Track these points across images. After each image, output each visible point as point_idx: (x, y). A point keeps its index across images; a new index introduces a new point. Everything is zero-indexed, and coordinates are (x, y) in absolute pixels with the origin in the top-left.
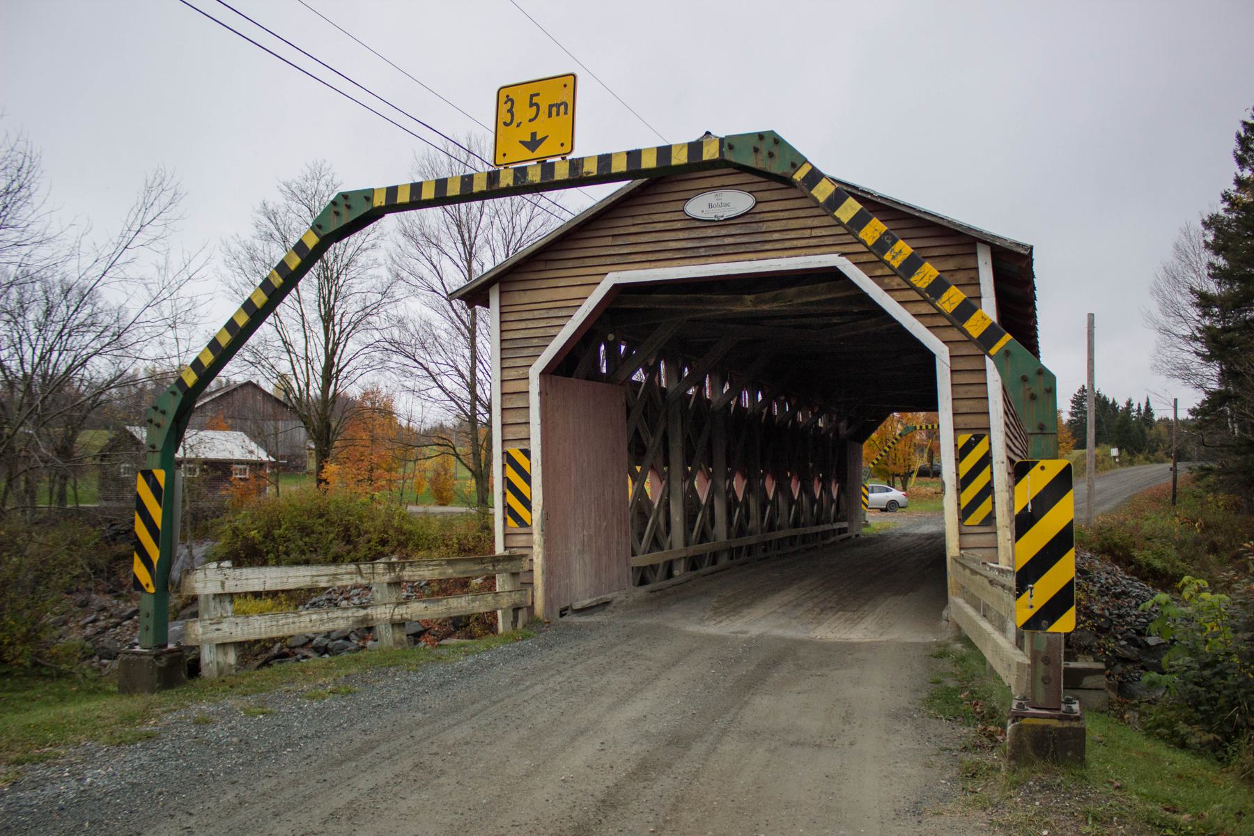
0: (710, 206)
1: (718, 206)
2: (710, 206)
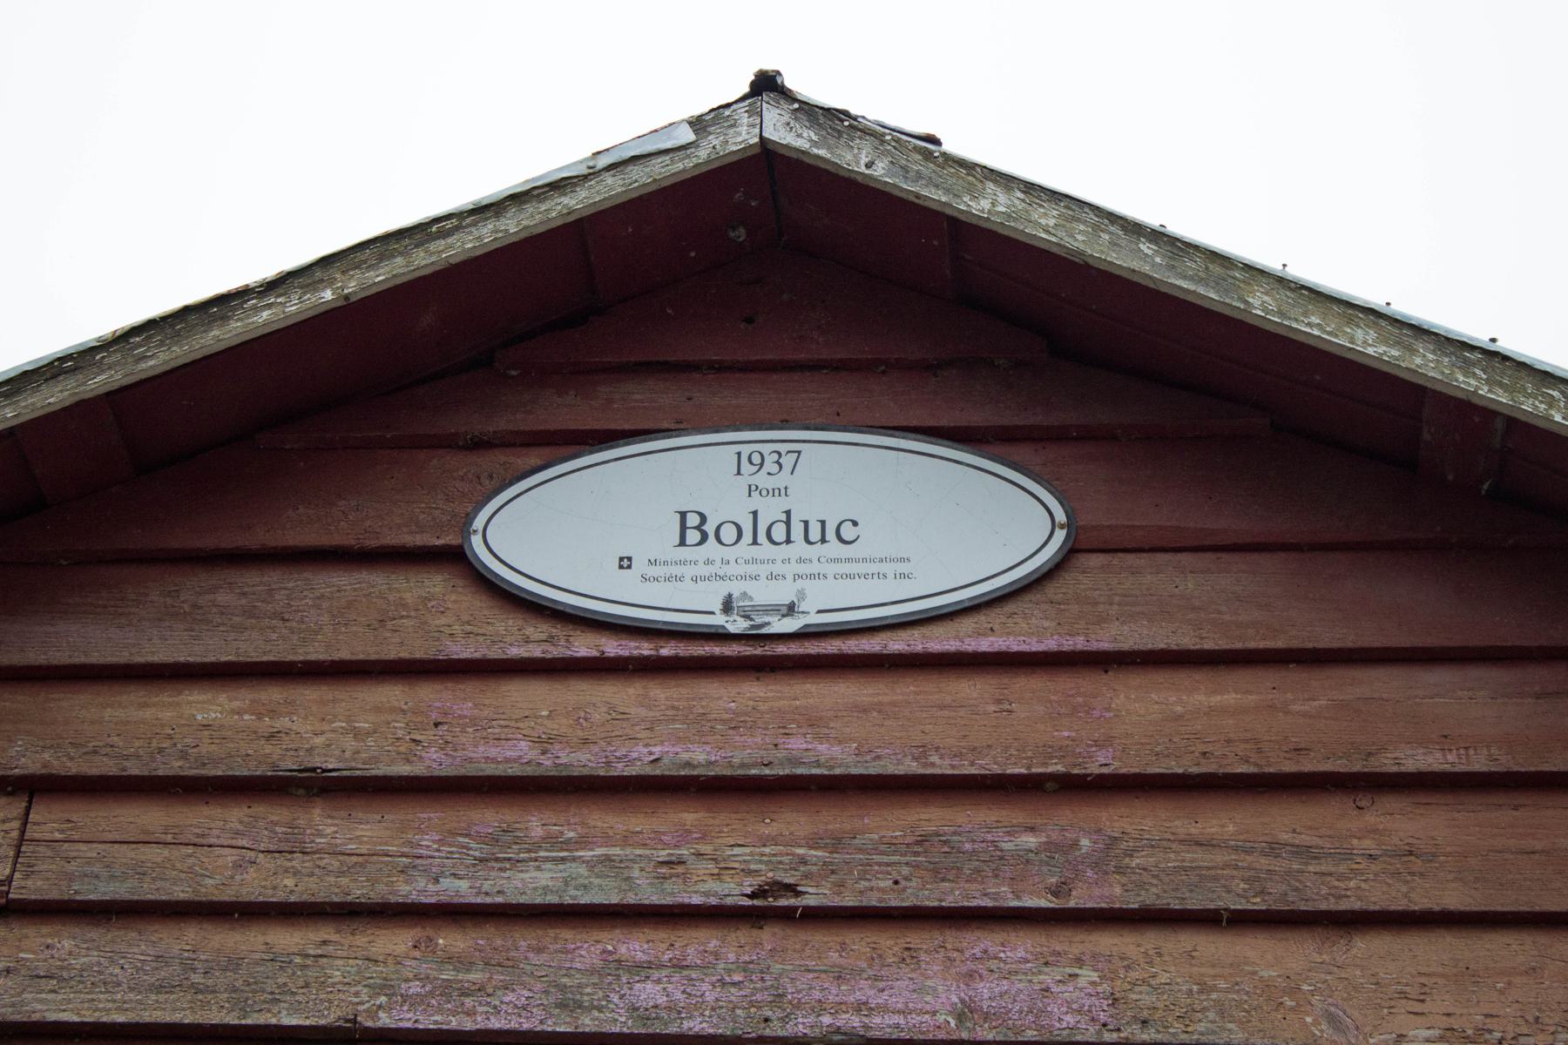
0: (693, 528)
1: (756, 532)
2: (693, 528)
